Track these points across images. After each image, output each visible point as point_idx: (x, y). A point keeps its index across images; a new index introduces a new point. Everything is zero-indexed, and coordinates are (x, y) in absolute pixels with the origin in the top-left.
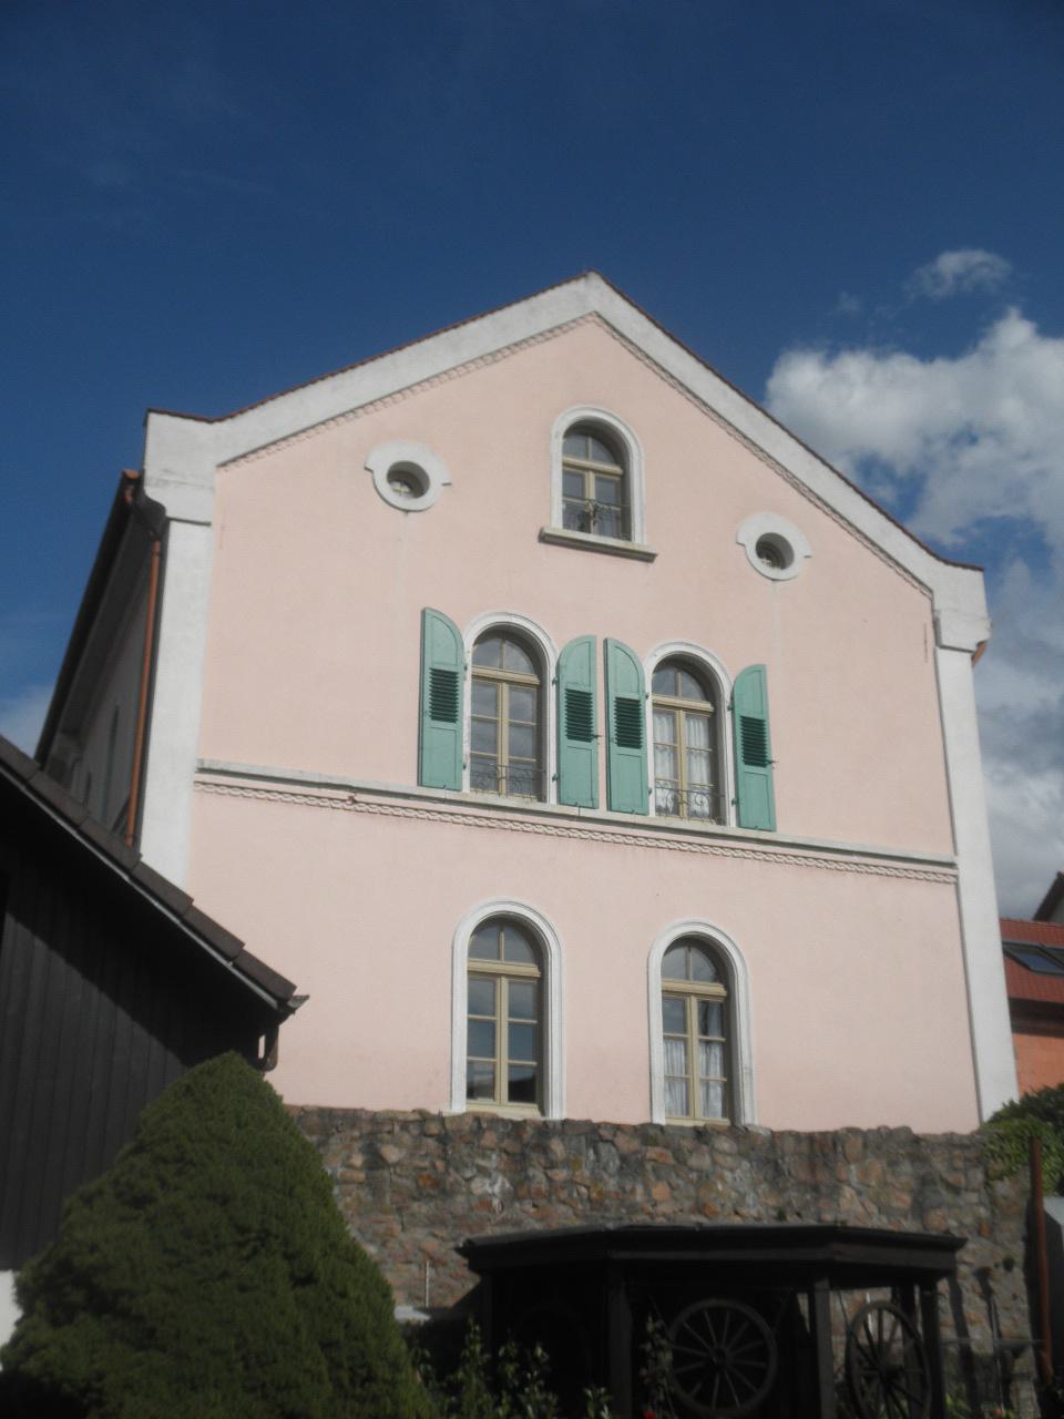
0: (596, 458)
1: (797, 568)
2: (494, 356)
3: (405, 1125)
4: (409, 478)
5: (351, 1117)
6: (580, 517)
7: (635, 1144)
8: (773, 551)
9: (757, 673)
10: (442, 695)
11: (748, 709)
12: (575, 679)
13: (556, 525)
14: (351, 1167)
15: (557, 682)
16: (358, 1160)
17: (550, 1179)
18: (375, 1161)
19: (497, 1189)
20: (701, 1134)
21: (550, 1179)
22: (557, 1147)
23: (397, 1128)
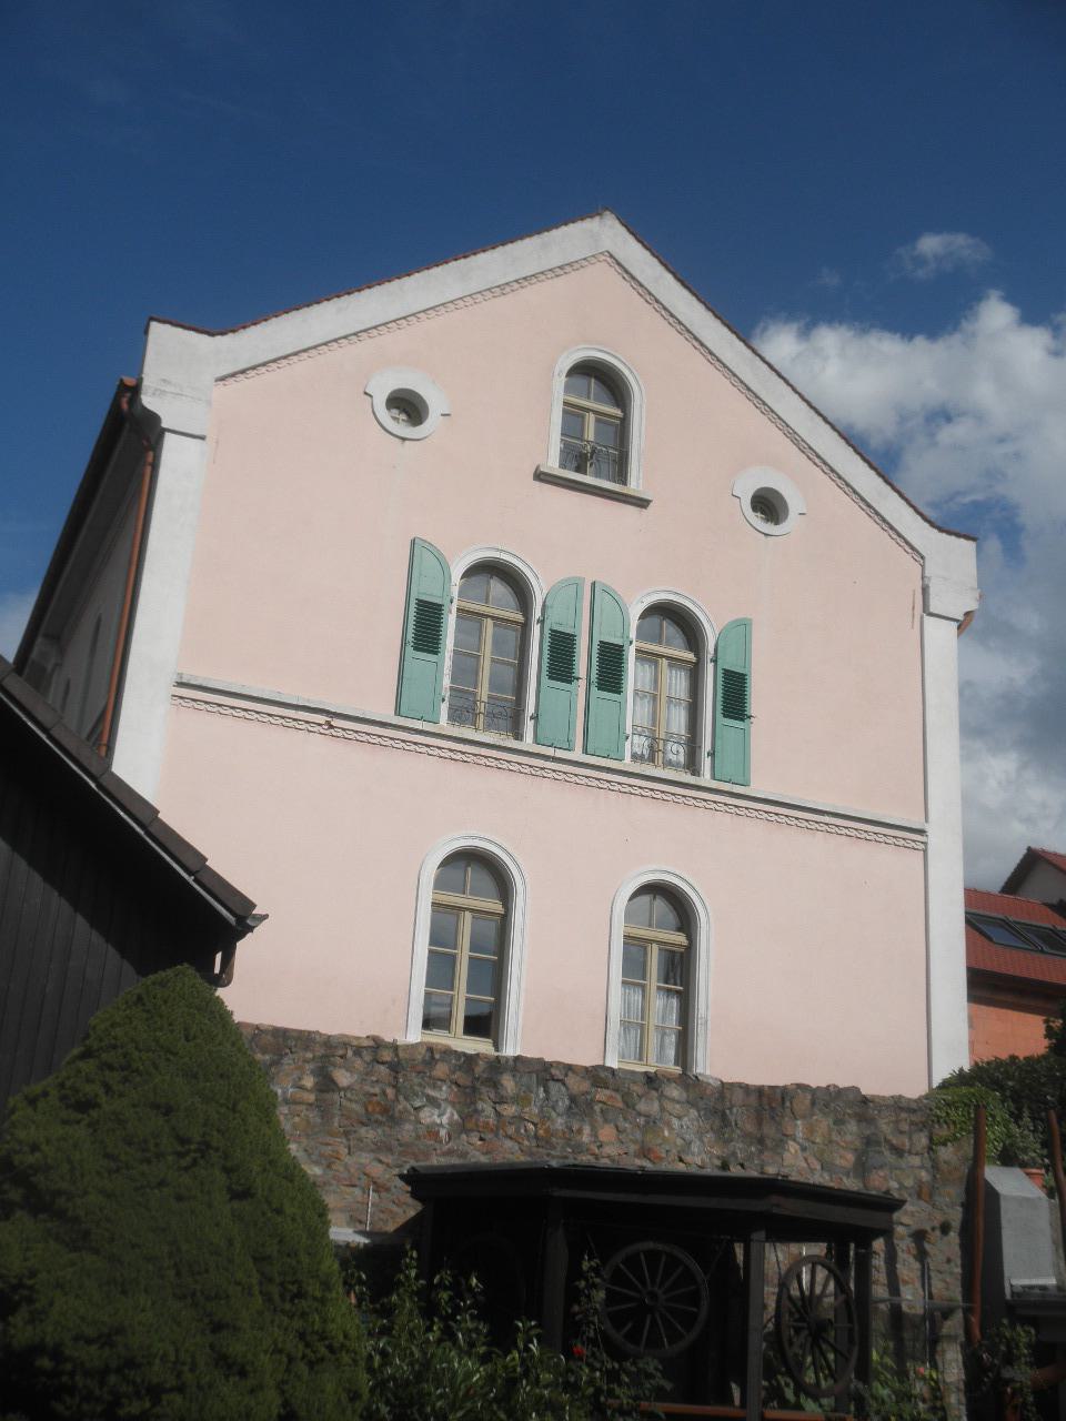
0: (597, 400)
1: (791, 523)
2: (503, 288)
3: (358, 1051)
4: (408, 406)
5: (305, 1039)
6: (577, 457)
7: (585, 1086)
8: (768, 505)
9: (743, 627)
10: (425, 626)
11: (731, 662)
12: (560, 620)
13: (553, 464)
14: (302, 1088)
15: (542, 622)
16: (309, 1082)
17: (498, 1114)
18: (326, 1084)
19: (445, 1120)
20: (651, 1080)
21: (498, 1114)
22: (508, 1084)
23: (350, 1053)
